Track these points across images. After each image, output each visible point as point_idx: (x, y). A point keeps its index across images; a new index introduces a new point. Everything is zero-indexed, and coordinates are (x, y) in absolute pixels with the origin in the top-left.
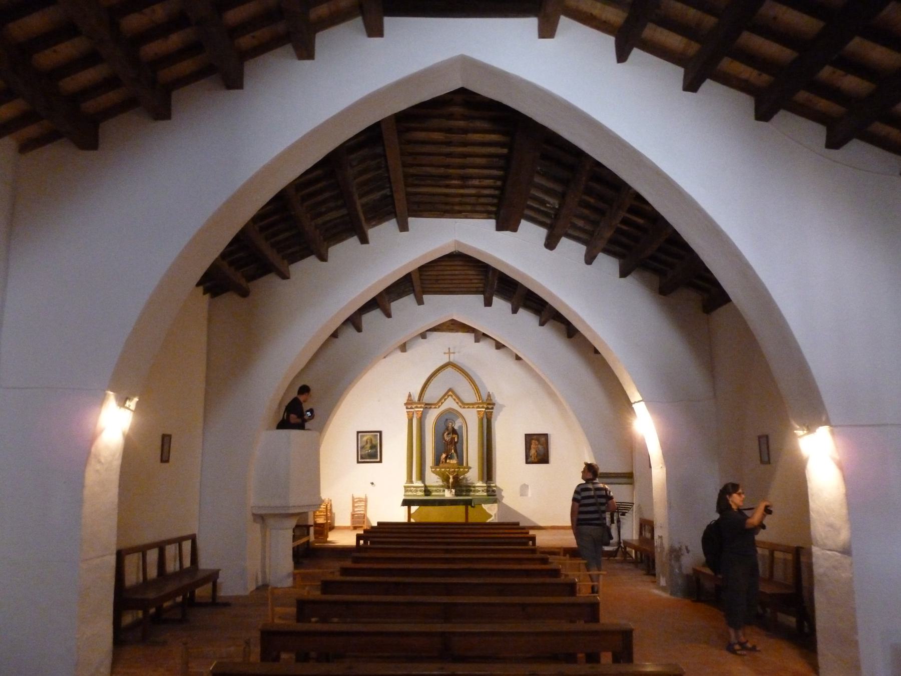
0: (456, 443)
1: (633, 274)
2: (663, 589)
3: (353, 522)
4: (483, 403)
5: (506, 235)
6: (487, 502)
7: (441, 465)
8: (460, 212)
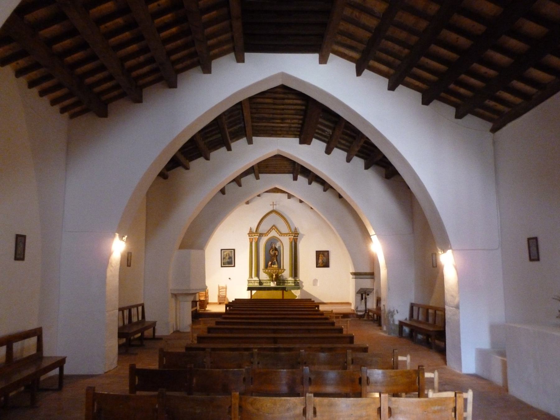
0: (277, 256)
1: (371, 168)
2: (385, 332)
3: (219, 300)
4: (292, 233)
5: (305, 146)
6: (294, 288)
7: (268, 268)
8: (281, 134)
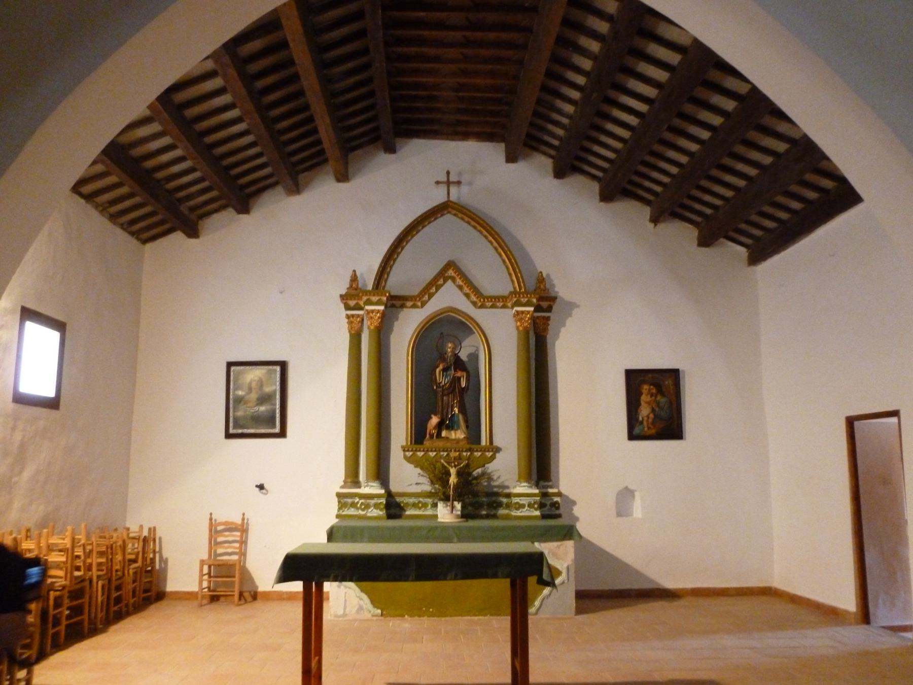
7: (427, 443)
